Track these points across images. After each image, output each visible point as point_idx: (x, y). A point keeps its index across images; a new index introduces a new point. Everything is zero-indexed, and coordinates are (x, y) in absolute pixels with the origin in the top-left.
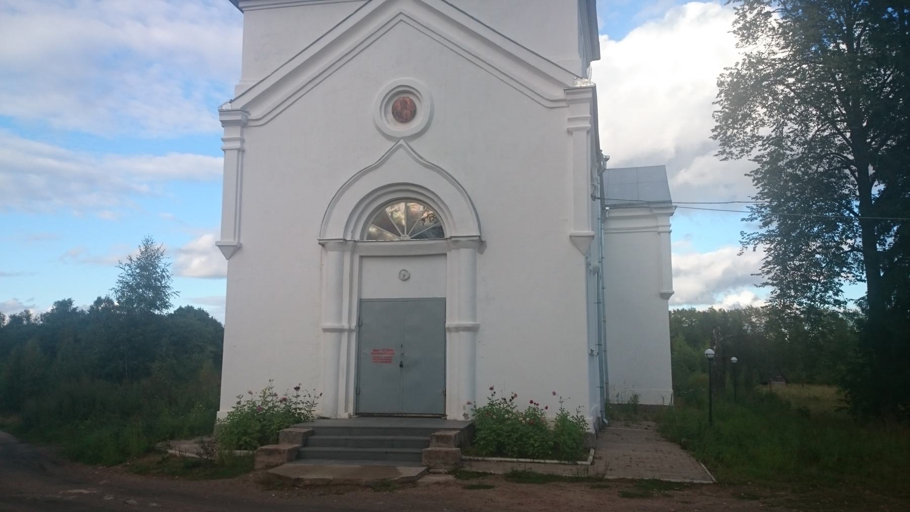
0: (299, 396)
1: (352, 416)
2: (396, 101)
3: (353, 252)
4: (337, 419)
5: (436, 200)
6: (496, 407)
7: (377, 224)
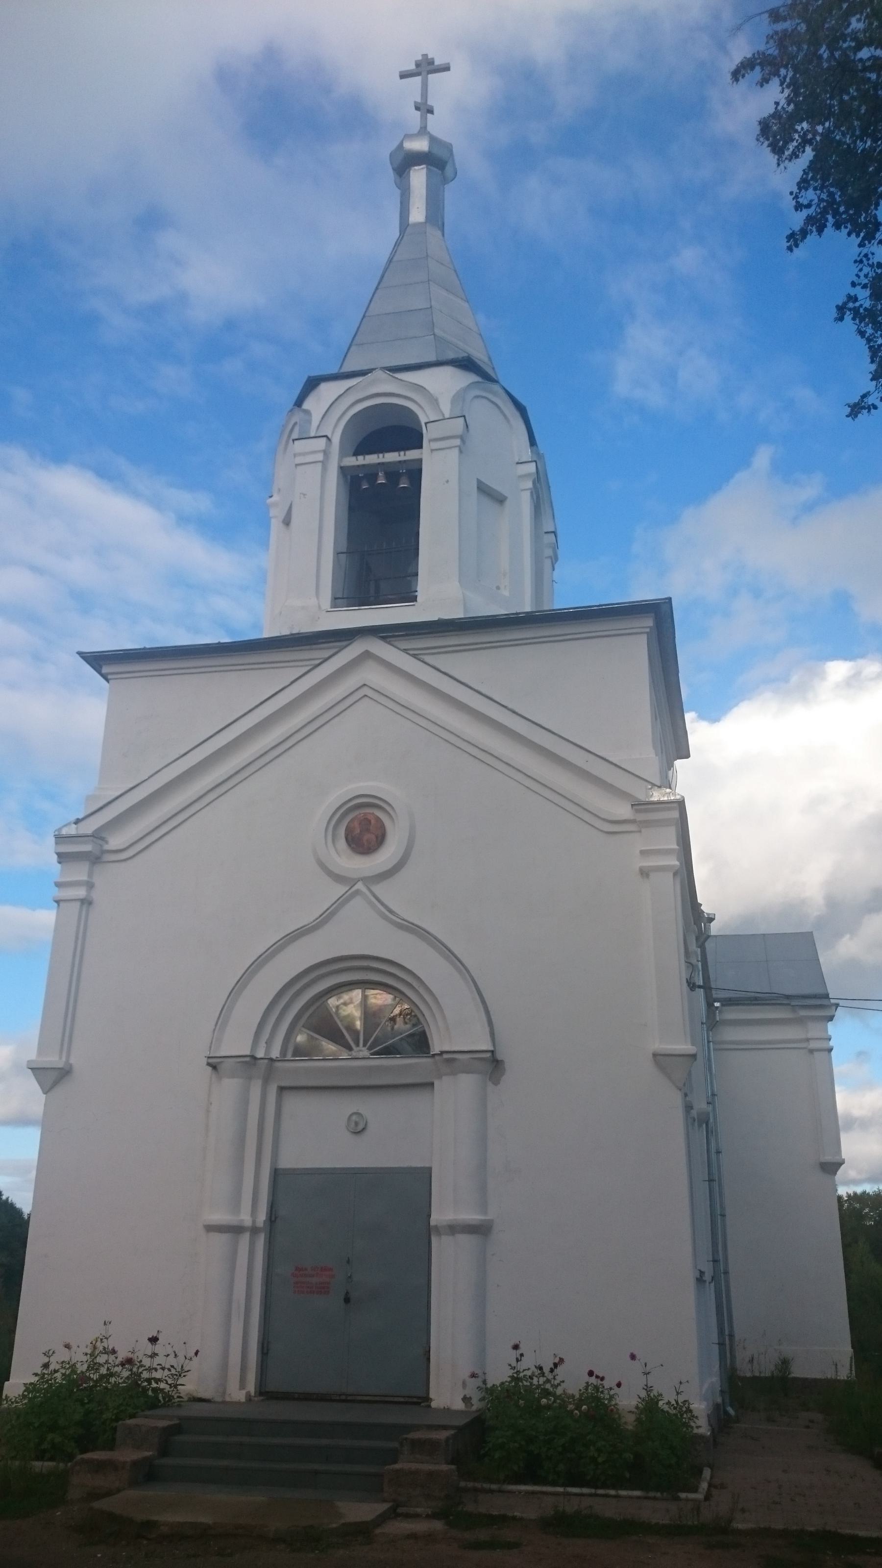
0: (157, 1355)
1: (253, 1398)
2: (352, 821)
3: (266, 1081)
4: (224, 1402)
5: (415, 984)
6: (525, 1383)
7: (309, 1026)
